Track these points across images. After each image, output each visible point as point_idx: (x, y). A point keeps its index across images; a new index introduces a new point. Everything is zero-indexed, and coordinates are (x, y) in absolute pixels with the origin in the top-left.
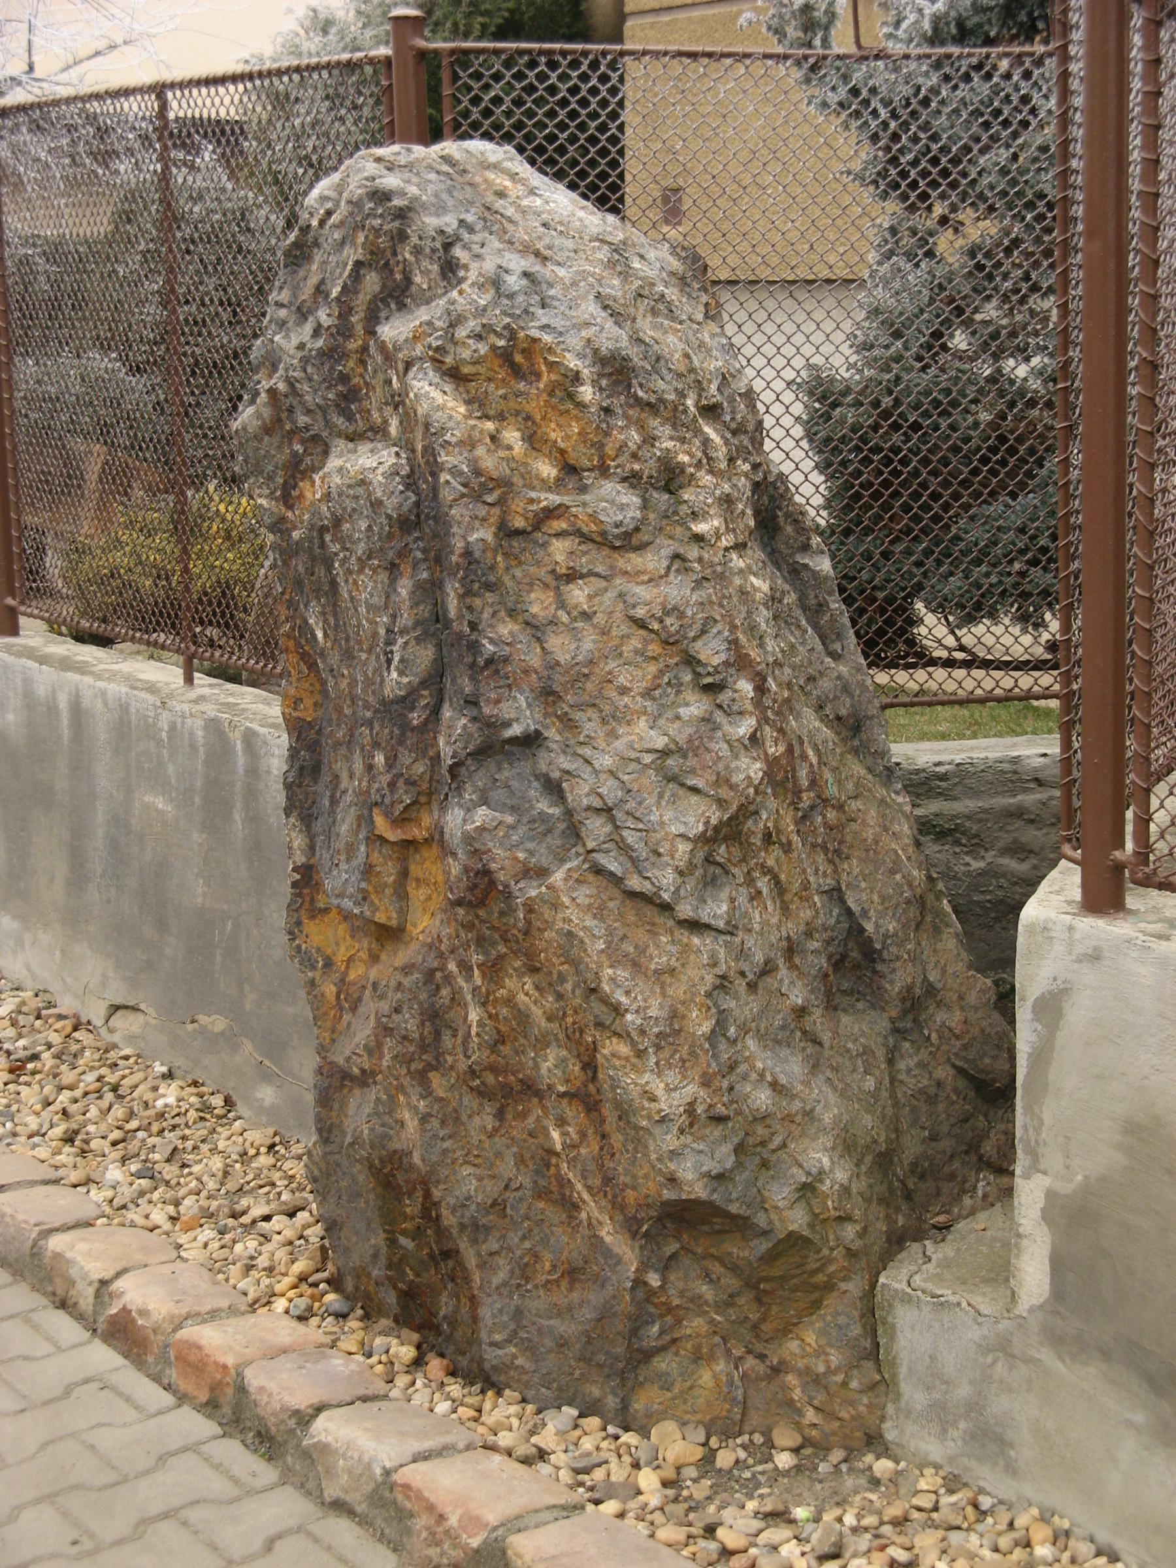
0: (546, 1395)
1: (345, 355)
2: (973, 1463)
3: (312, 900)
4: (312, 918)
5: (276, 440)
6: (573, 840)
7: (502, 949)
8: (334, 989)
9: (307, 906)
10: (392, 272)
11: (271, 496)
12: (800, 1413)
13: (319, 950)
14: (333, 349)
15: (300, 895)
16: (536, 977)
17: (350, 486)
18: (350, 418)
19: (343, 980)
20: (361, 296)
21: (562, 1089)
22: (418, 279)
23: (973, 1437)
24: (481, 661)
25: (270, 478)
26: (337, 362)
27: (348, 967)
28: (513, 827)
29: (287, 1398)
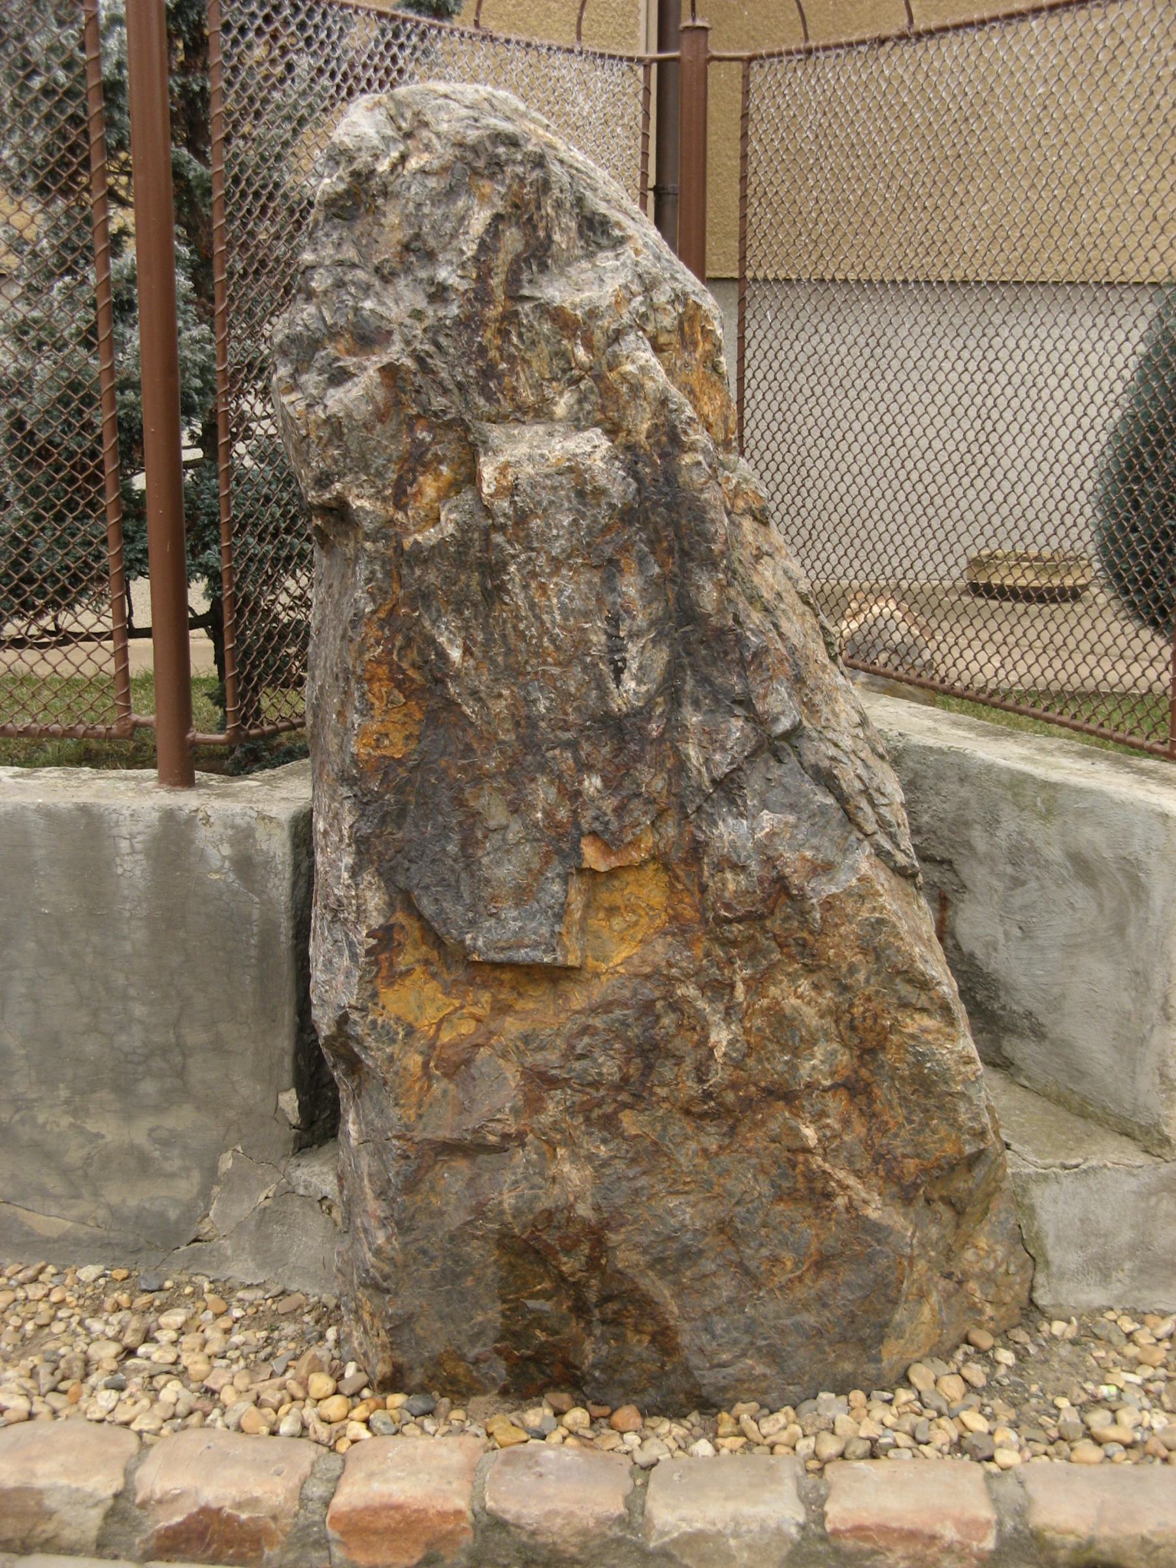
0: (793, 1389)
1: (483, 324)
2: (1145, 1293)
3: (391, 965)
4: (391, 984)
5: (391, 426)
6: (850, 827)
7: (776, 956)
8: (419, 1059)
9: (384, 973)
10: (535, 228)
11: (378, 495)
12: (981, 1312)
13: (398, 1019)
14: (470, 318)
15: (376, 963)
16: (814, 978)
17: (547, 476)
18: (490, 397)
19: (432, 1046)
20: (501, 255)
21: (827, 1083)
22: (557, 237)
23: (1141, 1271)
24: (748, 656)
25: (379, 474)
26: (475, 332)
27: (438, 1029)
28: (796, 826)
29: (597, 1509)
